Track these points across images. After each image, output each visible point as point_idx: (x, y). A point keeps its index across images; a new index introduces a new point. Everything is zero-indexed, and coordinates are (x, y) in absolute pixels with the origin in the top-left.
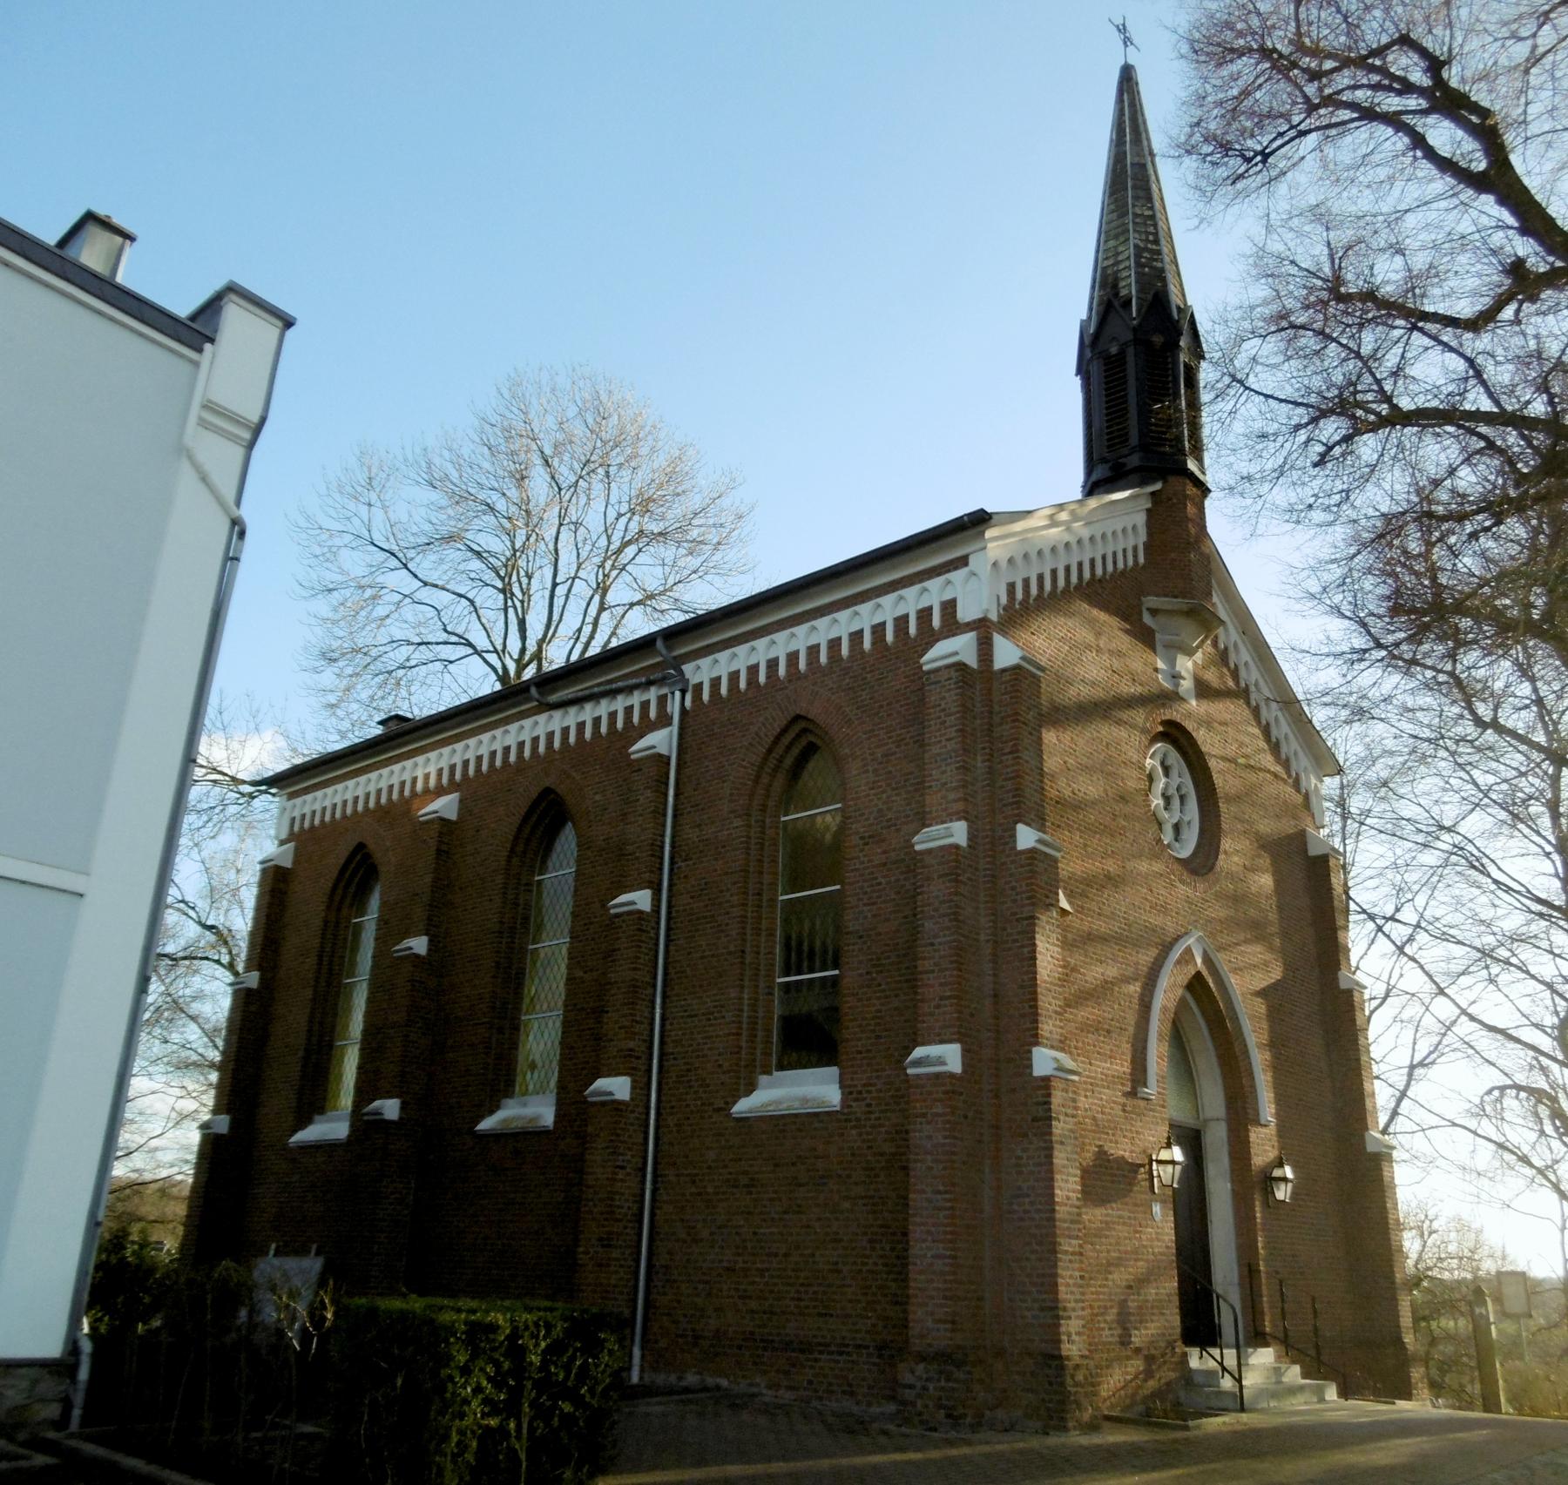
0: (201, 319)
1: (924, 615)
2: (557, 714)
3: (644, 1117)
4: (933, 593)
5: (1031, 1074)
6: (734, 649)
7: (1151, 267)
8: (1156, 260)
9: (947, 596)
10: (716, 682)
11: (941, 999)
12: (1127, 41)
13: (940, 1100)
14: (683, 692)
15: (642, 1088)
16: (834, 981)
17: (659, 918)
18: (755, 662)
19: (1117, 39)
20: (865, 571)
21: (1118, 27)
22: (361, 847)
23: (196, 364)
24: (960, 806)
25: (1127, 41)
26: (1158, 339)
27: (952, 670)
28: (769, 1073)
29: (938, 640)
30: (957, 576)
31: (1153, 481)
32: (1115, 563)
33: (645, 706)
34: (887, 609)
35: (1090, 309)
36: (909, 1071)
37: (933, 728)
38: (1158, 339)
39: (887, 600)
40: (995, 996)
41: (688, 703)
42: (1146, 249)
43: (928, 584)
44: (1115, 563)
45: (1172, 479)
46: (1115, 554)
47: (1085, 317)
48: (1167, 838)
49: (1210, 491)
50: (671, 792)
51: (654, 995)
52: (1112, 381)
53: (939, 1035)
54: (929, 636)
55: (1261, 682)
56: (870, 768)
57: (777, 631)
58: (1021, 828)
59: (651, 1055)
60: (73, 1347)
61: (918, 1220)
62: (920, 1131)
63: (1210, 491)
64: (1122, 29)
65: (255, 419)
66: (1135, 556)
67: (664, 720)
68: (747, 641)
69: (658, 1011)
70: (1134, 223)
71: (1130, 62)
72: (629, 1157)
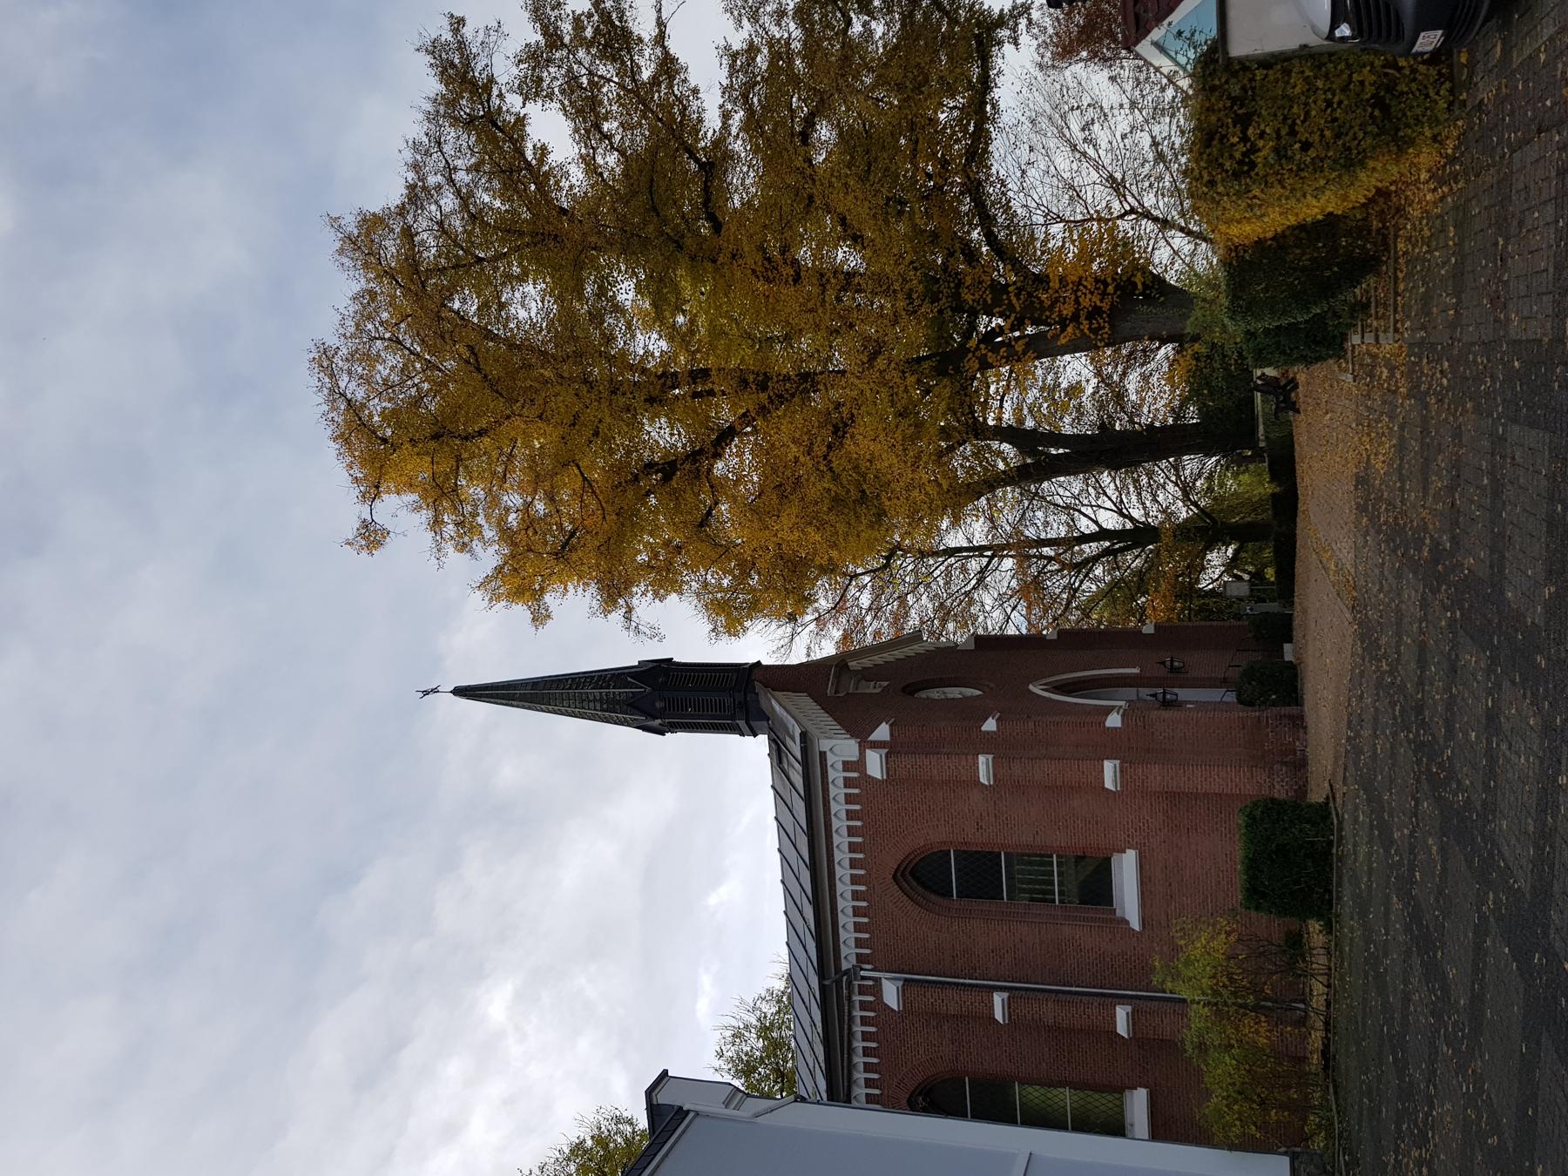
4: (836, 775)
7: (609, 681)
9: (840, 766)
12: (435, 691)
14: (862, 969)
16: (1045, 897)
18: (851, 910)
20: (814, 818)
23: (697, 1114)
24: (970, 757)
25: (435, 691)
28: (1115, 910)
30: (831, 759)
33: (864, 1006)
41: (869, 967)
42: (597, 682)
52: (1389, 31)
58: (983, 728)
60: (1285, 1154)
61: (1199, 787)
64: (426, 693)
71: (452, 689)
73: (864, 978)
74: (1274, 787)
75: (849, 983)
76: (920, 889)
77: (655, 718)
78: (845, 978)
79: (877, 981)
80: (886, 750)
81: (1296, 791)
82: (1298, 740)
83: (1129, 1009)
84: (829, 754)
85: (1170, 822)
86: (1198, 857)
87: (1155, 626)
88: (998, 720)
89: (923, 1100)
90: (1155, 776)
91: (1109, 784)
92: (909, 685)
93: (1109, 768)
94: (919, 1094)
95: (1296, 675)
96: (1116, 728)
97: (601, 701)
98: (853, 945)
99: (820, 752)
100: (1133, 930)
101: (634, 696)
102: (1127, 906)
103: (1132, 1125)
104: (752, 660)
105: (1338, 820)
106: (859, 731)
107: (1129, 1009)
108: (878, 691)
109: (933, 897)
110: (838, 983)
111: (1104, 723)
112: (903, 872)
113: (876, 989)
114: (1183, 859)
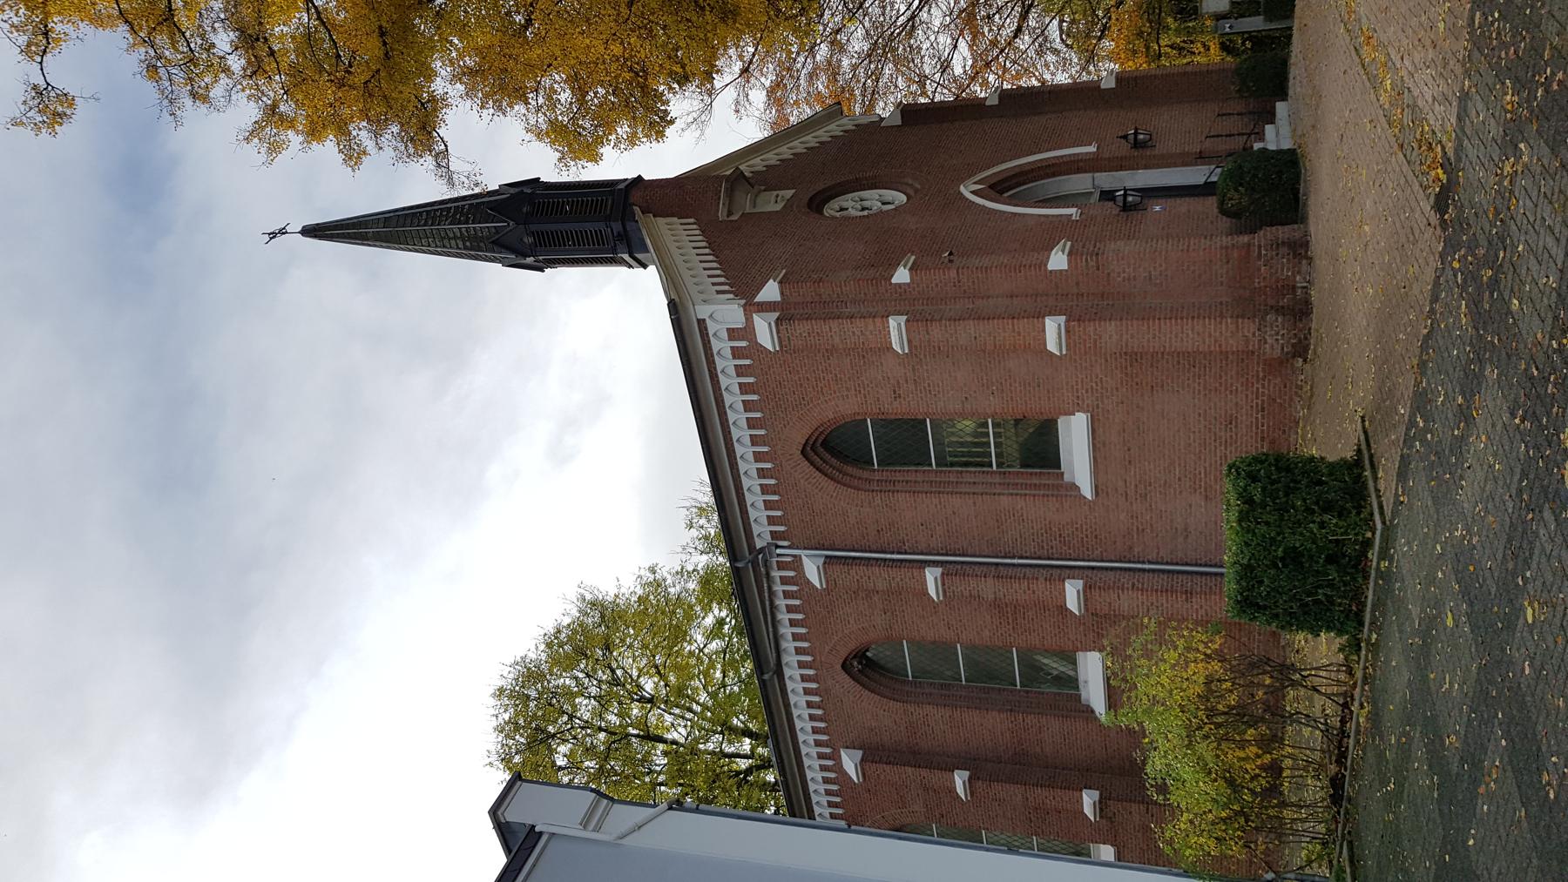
0: (511, 844)
2: (785, 659)
4: (721, 345)
5: (1066, 271)
11: (1014, 331)
12: (282, 232)
13: (1084, 329)
14: (777, 547)
15: (1073, 572)
17: (947, 562)
21: (271, 238)
25: (282, 232)
27: (781, 328)
28: (1062, 474)
30: (712, 327)
36: (1064, 352)
37: (821, 341)
39: (724, 381)
40: (1012, 297)
41: (785, 543)
49: (640, 176)
52: (562, 235)
54: (755, 349)
58: (894, 281)
61: (1167, 345)
62: (1106, 343)
63: (640, 176)
64: (273, 235)
70: (432, 225)
73: (778, 555)
74: (1266, 343)
75: (766, 562)
76: (834, 461)
77: (525, 256)
78: (760, 556)
79: (798, 559)
80: (777, 314)
81: (1293, 345)
82: (1299, 272)
83: (1080, 584)
84: (708, 321)
85: (1129, 380)
86: (1163, 418)
88: (911, 269)
89: (860, 663)
90: (1110, 333)
91: (1052, 346)
93: (1053, 328)
94: (855, 657)
95: (1298, 175)
97: (462, 238)
98: (766, 523)
99: (699, 321)
100: (1085, 498)
101: (497, 232)
102: (1076, 459)
103: (1086, 682)
104: (631, 175)
105: (1384, 523)
106: (743, 288)
107: (1080, 584)
108: (778, 207)
109: (849, 469)
110: (755, 563)
111: (1046, 265)
112: (815, 442)
113: (796, 564)
114: (1145, 420)
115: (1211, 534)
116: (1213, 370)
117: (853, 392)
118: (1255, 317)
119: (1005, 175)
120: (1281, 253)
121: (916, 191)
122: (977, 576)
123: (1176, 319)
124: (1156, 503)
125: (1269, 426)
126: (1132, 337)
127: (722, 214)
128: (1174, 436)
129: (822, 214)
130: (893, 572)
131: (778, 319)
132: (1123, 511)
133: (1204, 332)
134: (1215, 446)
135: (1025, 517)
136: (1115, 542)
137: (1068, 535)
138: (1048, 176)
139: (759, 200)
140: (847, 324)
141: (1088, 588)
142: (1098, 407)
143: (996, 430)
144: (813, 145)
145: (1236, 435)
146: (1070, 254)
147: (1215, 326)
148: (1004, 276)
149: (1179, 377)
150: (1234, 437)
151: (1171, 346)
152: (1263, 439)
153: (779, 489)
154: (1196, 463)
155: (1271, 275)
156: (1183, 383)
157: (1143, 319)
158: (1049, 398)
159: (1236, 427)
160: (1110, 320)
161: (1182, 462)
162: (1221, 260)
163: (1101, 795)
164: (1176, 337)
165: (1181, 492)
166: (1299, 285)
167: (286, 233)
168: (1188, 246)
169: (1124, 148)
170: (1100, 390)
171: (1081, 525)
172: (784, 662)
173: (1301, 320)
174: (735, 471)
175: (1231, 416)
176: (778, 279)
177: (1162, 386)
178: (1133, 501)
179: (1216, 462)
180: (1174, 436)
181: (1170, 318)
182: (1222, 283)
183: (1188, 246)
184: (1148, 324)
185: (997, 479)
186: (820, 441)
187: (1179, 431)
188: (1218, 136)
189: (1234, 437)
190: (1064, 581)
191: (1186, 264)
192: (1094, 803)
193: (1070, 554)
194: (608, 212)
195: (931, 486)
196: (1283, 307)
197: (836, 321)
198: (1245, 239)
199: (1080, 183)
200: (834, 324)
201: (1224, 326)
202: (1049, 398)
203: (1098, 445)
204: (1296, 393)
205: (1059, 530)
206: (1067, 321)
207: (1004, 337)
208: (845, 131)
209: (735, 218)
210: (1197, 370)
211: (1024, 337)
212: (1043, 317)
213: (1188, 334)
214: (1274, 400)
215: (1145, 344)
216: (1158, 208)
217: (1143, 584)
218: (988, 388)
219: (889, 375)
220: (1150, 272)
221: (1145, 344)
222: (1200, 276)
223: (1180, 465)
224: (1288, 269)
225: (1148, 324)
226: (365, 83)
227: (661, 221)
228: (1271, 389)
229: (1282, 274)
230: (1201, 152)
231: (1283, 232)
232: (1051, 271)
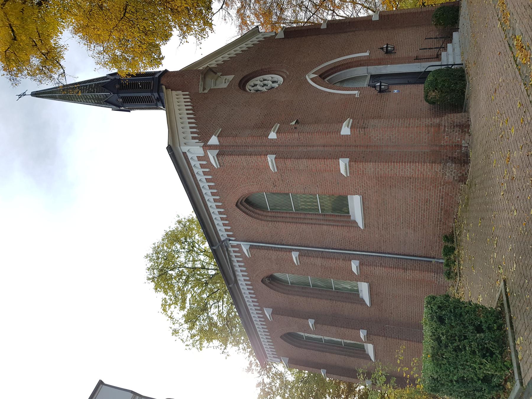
1: (202, 166)
2: (238, 278)
3: (365, 256)
4: (195, 163)
5: (350, 135)
6: (216, 225)
7: (94, 88)
8: (92, 86)
10: (226, 230)
12: (24, 94)
14: (230, 240)
15: (355, 257)
19: (23, 98)
21: (20, 98)
22: (281, 337)
25: (24, 94)
26: (118, 86)
27: (219, 158)
28: (350, 216)
29: (211, 162)
30: (189, 156)
31: (162, 88)
32: (188, 102)
34: (201, 178)
35: (108, 107)
38: (118, 86)
40: (324, 146)
42: (89, 88)
43: (192, 164)
44: (188, 102)
45: (162, 82)
46: (185, 102)
47: (111, 109)
48: (276, 85)
50: (261, 244)
51: (326, 252)
53: (336, 165)
55: (228, 53)
56: (252, 184)
57: (209, 211)
58: (269, 137)
59: (344, 253)
63: (166, 70)
64: (20, 96)
65: (132, 395)
66: (186, 95)
67: (239, 246)
68: (213, 221)
69: (330, 250)
71: (30, 94)
72: (378, 261)
74: (446, 175)
76: (251, 208)
77: (120, 107)
81: (459, 177)
82: (464, 139)
83: (358, 262)
84: (188, 153)
86: (395, 198)
87: (379, 15)
90: (370, 168)
92: (241, 81)
95: (465, 85)
96: (347, 135)
107: (358, 262)
108: (225, 86)
109: (258, 211)
111: (340, 132)
115: (416, 244)
116: (419, 180)
117: (255, 183)
118: (441, 163)
119: (326, 69)
120: (455, 130)
121: (287, 76)
122: (313, 257)
123: (402, 162)
124: (392, 231)
125: (445, 204)
126: (381, 169)
127: (201, 91)
128: (400, 206)
129: (244, 89)
130: (278, 253)
131: (217, 154)
132: (377, 234)
133: (416, 169)
134: (419, 211)
135: (334, 234)
136: (373, 245)
137: (353, 241)
138: (347, 68)
139: (218, 82)
140: (249, 158)
141: (361, 264)
142: (365, 194)
143: (321, 201)
144: (244, 49)
145: (429, 207)
146: (351, 128)
147: (421, 166)
148: (320, 137)
149: (403, 182)
150: (428, 208)
151: (399, 174)
152: (442, 209)
153: (228, 219)
154: (410, 217)
155: (450, 140)
156: (405, 185)
157: (386, 162)
158: (343, 189)
159: (429, 204)
160: (370, 162)
161: (404, 216)
162: (425, 132)
163: (367, 332)
164: (402, 170)
165: (403, 228)
166: (463, 145)
167: (25, 95)
168: (409, 124)
169: (381, 54)
170: (366, 186)
171: (359, 238)
172: (238, 279)
173: (464, 166)
174: (208, 212)
175: (427, 199)
176: (217, 135)
177: (395, 186)
178: (382, 230)
179: (419, 217)
180: (400, 206)
181: (399, 162)
182: (425, 143)
183: (409, 124)
184: (388, 164)
185: (321, 217)
186: (244, 200)
187: (402, 204)
188: (427, 59)
189: (428, 208)
190: (351, 261)
191: (408, 134)
192: (365, 336)
193: (354, 248)
194: (152, 88)
195: (293, 220)
196: (455, 158)
197: (243, 156)
198: (437, 121)
199: (361, 71)
200: (243, 158)
201: (425, 167)
202: (343, 189)
203: (365, 208)
204: (459, 192)
205: (349, 239)
206: (350, 161)
207: (320, 166)
208: (253, 44)
209: (206, 91)
210: (412, 180)
211: (330, 167)
212: (338, 159)
213: (407, 170)
214: (448, 194)
215: (387, 173)
216: (396, 91)
217: (385, 264)
218: (315, 184)
219: (271, 177)
220: (390, 137)
221: (387, 173)
222: (415, 139)
223: (403, 218)
224: (458, 138)
225: (388, 164)
226: (6, 51)
227: (174, 93)
228: (447, 190)
229: (455, 139)
230: (417, 57)
231: (456, 117)
232: (342, 135)
